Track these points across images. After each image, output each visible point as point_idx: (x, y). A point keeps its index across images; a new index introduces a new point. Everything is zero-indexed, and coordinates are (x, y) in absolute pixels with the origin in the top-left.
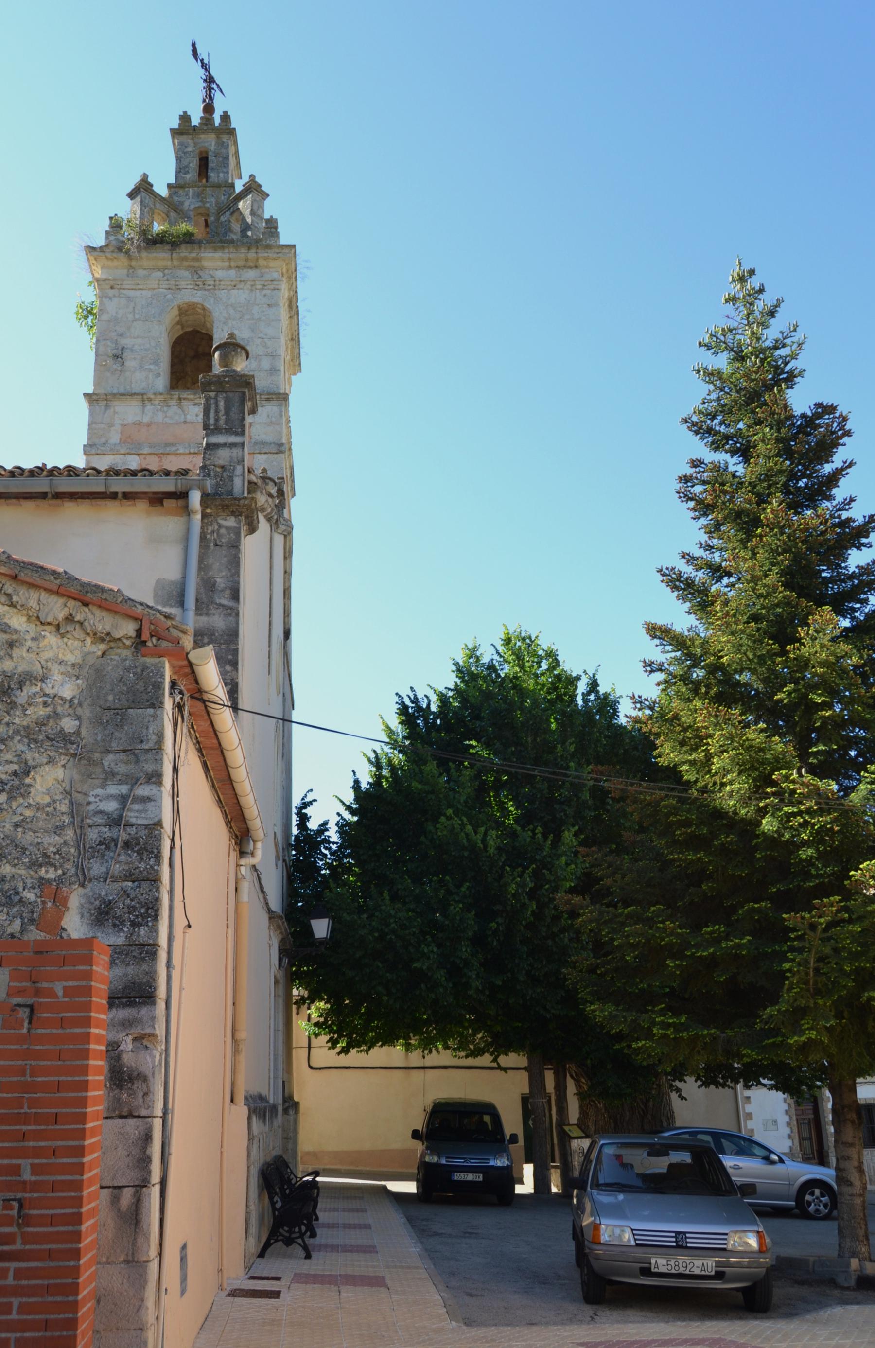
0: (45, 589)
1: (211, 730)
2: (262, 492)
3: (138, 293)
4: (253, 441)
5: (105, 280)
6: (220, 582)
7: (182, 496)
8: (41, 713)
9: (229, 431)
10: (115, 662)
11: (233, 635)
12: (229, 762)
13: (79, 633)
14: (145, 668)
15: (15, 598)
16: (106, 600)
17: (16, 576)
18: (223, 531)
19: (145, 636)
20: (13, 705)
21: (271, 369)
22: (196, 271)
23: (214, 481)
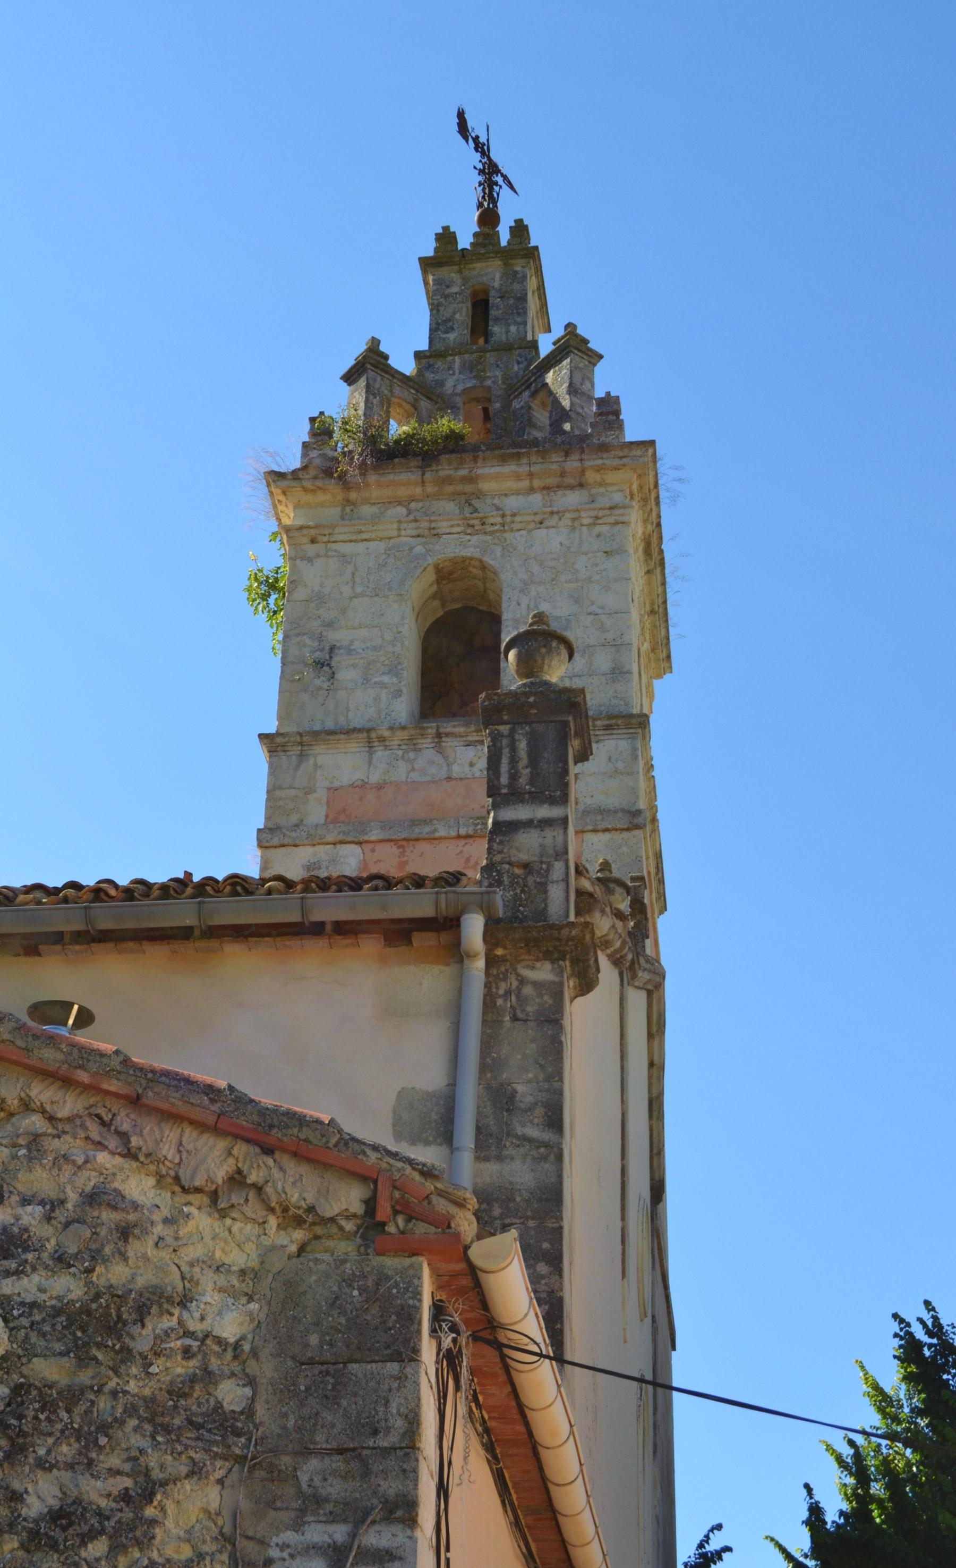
0: (192, 1122)
1: (513, 1404)
2: (603, 912)
3: (361, 547)
4: (581, 807)
5: (300, 528)
6: (524, 1091)
7: (449, 924)
8: (179, 1370)
9: (537, 797)
10: (323, 1267)
11: (551, 1198)
12: (550, 1473)
13: (253, 1209)
14: (382, 1278)
15: (134, 1141)
16: (307, 1141)
17: (138, 1097)
18: (528, 990)
19: (384, 1210)
20: (126, 1354)
21: (613, 671)
22: (469, 500)
23: (509, 894)
